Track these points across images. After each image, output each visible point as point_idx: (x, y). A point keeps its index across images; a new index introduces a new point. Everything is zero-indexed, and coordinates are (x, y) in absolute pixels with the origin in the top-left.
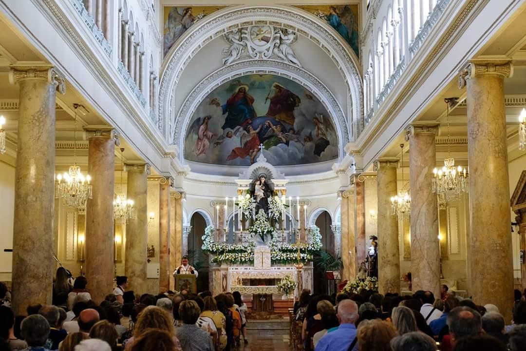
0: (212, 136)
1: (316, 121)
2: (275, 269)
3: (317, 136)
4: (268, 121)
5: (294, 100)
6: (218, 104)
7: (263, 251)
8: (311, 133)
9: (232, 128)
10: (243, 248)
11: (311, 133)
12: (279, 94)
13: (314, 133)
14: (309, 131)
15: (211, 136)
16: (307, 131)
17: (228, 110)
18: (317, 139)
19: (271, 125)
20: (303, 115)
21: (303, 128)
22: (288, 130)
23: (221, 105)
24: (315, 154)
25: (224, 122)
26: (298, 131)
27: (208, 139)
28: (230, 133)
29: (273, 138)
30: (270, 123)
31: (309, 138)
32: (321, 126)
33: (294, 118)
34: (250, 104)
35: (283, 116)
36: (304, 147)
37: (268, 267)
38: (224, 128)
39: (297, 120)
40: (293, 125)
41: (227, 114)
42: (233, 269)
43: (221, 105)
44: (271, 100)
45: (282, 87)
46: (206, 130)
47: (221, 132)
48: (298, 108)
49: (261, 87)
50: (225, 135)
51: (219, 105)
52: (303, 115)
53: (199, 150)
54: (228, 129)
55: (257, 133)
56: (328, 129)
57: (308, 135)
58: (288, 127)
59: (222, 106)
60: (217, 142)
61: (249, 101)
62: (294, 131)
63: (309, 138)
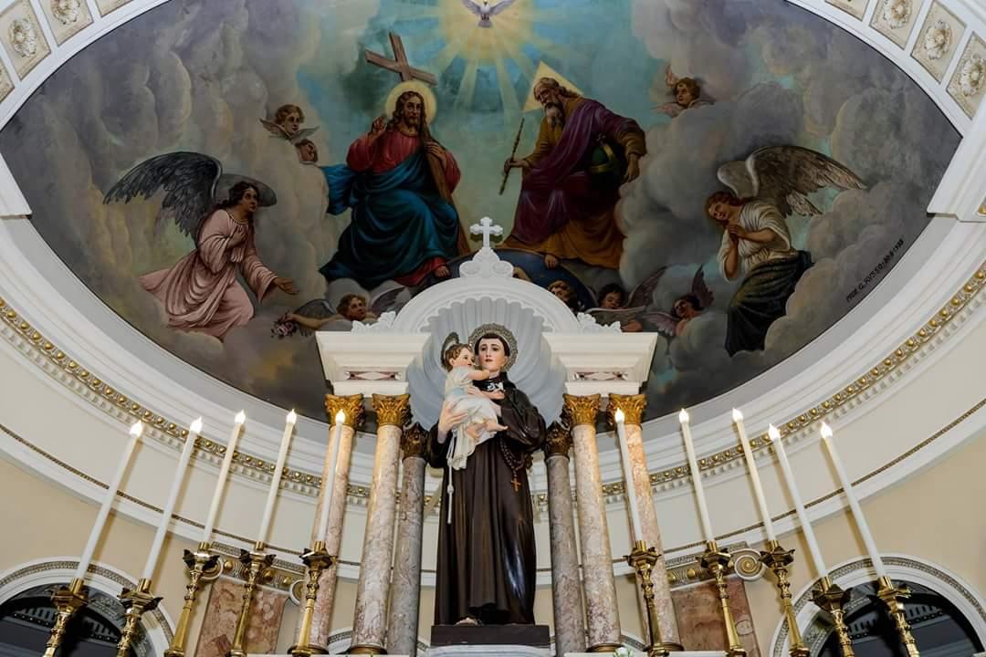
0: (272, 285)
1: (724, 207)
5: (619, 150)
6: (308, 152)
8: (700, 274)
9: (369, 285)
11: (700, 274)
12: (558, 135)
13: (716, 266)
14: (692, 270)
15: (265, 285)
16: (680, 275)
17: (353, 200)
18: (733, 284)
22: (595, 298)
23: (322, 161)
24: (732, 349)
25: (333, 249)
26: (642, 288)
27: (253, 290)
28: (355, 301)
31: (697, 298)
33: (619, 237)
34: (443, 190)
35: (574, 240)
36: (674, 343)
38: (330, 272)
39: (631, 244)
40: (616, 270)
41: (345, 218)
43: (322, 161)
44: (525, 170)
45: (570, 87)
46: (246, 242)
47: (315, 286)
48: (637, 182)
49: (486, 102)
50: (334, 305)
51: (315, 159)
53: (190, 310)
54: (349, 286)
56: (791, 199)
57: (686, 288)
58: (593, 281)
59: (325, 170)
60: (294, 321)
61: (438, 175)
62: (623, 294)
63: (697, 298)
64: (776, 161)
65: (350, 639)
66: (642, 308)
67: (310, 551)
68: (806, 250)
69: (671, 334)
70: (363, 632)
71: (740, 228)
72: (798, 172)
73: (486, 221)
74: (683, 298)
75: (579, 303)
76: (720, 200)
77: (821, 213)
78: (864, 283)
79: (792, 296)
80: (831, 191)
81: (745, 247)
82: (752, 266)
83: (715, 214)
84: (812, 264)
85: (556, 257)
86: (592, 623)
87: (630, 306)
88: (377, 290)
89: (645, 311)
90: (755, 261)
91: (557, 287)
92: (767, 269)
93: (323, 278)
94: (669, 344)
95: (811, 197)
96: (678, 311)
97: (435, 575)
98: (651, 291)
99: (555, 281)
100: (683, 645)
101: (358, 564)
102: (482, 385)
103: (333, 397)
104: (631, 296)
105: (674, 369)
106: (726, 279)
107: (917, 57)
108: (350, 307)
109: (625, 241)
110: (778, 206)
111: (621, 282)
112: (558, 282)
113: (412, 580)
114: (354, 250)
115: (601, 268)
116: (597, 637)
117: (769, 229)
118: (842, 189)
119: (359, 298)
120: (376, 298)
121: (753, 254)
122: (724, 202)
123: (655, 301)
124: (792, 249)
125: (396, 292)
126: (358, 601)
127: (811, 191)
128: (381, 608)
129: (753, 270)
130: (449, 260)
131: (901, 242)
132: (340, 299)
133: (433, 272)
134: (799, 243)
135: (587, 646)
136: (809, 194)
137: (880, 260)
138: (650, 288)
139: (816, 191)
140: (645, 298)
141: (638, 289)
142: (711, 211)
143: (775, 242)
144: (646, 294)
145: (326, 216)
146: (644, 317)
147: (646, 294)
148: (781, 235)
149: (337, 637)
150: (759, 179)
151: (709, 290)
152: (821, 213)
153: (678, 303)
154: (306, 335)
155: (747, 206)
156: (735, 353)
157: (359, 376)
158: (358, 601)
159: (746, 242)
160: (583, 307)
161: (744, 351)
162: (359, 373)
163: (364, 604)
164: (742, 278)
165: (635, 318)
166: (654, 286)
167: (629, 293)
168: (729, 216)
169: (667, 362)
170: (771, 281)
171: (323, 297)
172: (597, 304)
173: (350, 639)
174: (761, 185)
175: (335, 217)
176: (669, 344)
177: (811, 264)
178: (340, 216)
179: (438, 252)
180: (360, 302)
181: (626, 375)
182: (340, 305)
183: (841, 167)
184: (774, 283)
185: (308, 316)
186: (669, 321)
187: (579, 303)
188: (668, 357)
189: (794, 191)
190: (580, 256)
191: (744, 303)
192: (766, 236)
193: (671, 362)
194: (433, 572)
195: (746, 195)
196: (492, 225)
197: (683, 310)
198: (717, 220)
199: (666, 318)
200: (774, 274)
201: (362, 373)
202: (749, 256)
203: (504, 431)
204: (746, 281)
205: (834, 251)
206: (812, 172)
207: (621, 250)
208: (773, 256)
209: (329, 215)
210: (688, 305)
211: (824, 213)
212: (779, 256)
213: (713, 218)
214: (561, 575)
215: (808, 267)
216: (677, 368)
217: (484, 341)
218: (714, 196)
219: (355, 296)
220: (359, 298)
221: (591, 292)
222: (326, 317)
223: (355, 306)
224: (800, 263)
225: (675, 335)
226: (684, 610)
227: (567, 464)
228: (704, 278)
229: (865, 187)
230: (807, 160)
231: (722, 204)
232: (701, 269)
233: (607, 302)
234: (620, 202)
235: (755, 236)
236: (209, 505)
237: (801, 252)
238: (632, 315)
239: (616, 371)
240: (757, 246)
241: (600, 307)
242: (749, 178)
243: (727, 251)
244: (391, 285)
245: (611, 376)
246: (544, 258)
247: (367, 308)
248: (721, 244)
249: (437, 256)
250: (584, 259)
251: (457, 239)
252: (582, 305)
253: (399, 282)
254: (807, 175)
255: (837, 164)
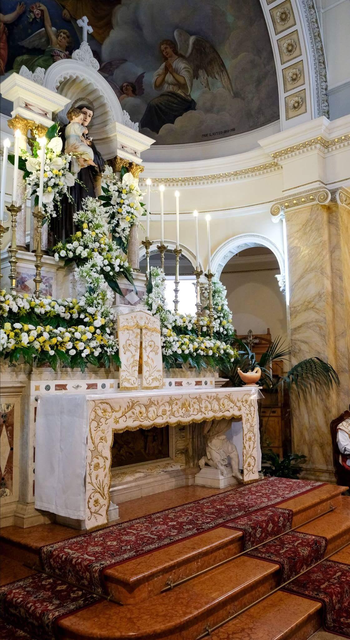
1: (169, 50)
2: (48, 388)
3: (159, 86)
4: (43, 7)
7: (142, 324)
8: (142, 76)
10: (60, 310)
11: (142, 76)
14: (140, 71)
19: (48, 22)
20: (137, 26)
21: (125, 60)
29: (44, 58)
30: (47, 15)
32: (180, 65)
37: (155, 379)
42: (48, 388)
52: (137, 26)
55: (6, 24)
56: (201, 72)
57: (133, 79)
64: (204, 49)
68: (195, 101)
71: (172, 66)
72: (210, 63)
74: (129, 83)
76: (169, 45)
77: (210, 90)
78: (212, 134)
79: (180, 117)
80: (219, 84)
81: (169, 78)
82: (169, 90)
83: (163, 51)
84: (195, 110)
85: (70, 14)
90: (171, 88)
92: (175, 96)
95: (210, 79)
96: (124, 88)
106: (154, 89)
107: (284, 72)
109: (112, 31)
110: (193, 71)
112: (66, 31)
117: (184, 77)
118: (224, 87)
121: (172, 84)
122: (171, 48)
124: (189, 95)
127: (211, 76)
129: (169, 92)
131: (234, 130)
134: (195, 95)
136: (210, 77)
137: (223, 130)
138: (115, 67)
139: (213, 78)
140: (110, 70)
141: (108, 63)
142: (163, 47)
143: (183, 86)
144: (111, 69)
147: (111, 69)
148: (188, 85)
150: (192, 51)
151: (143, 87)
152: (210, 90)
153: (125, 84)
155: (181, 58)
156: (143, 127)
159: (171, 76)
161: (148, 129)
164: (162, 92)
166: (117, 67)
168: (170, 57)
170: (174, 103)
174: (191, 54)
177: (194, 109)
183: (229, 77)
184: (175, 105)
189: (204, 70)
191: (157, 105)
192: (181, 80)
195: (183, 54)
197: (127, 89)
198: (163, 54)
200: (176, 101)
202: (169, 84)
204: (162, 95)
205: (209, 110)
206: (216, 68)
207: (108, 34)
208: (179, 92)
210: (130, 88)
211: (212, 91)
212: (183, 95)
213: (162, 52)
215: (192, 109)
218: (168, 40)
224: (190, 105)
228: (144, 79)
229: (233, 95)
230: (217, 61)
231: (169, 48)
232: (144, 73)
234: (119, 6)
235: (178, 77)
236: (177, 237)
237: (193, 100)
240: (176, 82)
242: (188, 45)
243: (160, 73)
248: (158, 68)
254: (213, 68)
255: (228, 75)
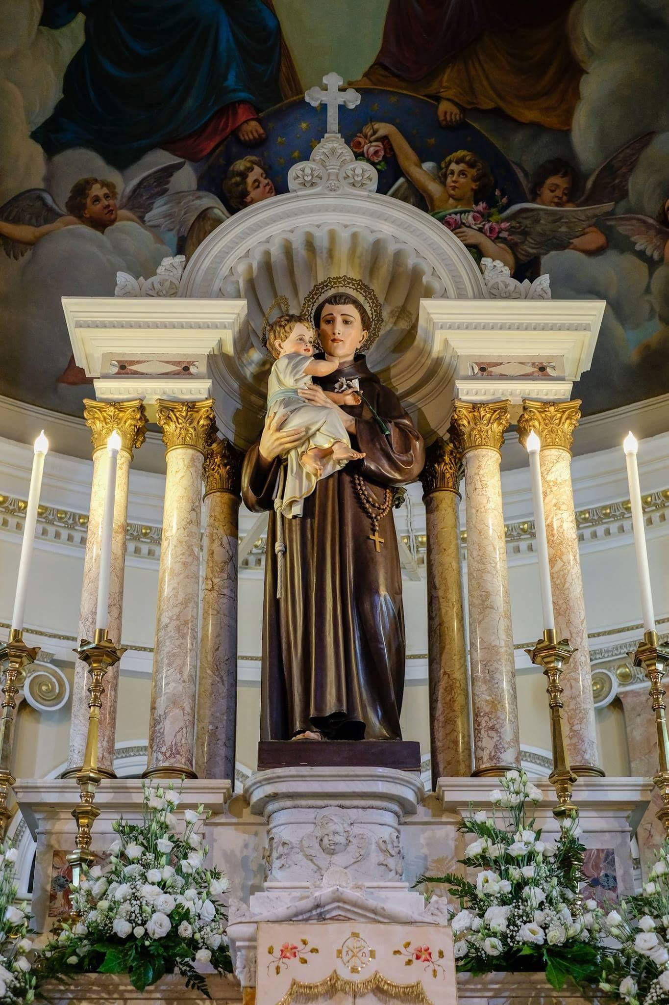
26: (609, 170)
28: (97, 190)
40: (565, 134)
50: (59, 200)
65: (146, 758)
66: (608, 206)
67: (89, 643)
69: (656, 256)
70: (163, 749)
73: (333, 80)
75: (497, 193)
86: (480, 740)
87: (586, 203)
88: (133, 168)
89: (612, 213)
91: (458, 162)
93: (38, 150)
94: (651, 275)
97: (239, 654)
98: (625, 177)
99: (456, 151)
100: (606, 773)
101: (151, 650)
102: (326, 383)
103: (94, 403)
104: (589, 184)
105: (656, 321)
108: (89, 201)
111: (573, 155)
112: (460, 153)
113: (225, 678)
114: (92, 94)
115: (537, 128)
116: (486, 757)
119: (104, 184)
120: (135, 181)
123: (630, 193)
125: (169, 171)
126: (153, 708)
128: (187, 718)
130: (262, 111)
132: (70, 187)
133: (235, 133)
135: (474, 768)
145: (39, 32)
146: (610, 223)
149: (127, 752)
154: (16, 258)
157: (134, 368)
158: (153, 708)
160: (505, 200)
162: (133, 363)
163: (162, 713)
165: (594, 225)
166: (632, 166)
167: (586, 177)
169: (647, 308)
171: (42, 185)
172: (529, 197)
173: (146, 758)
175: (56, 33)
176: (651, 275)
178: (65, 30)
179: (244, 95)
180: (105, 190)
181: (554, 368)
182: (71, 198)
185: (17, 220)
186: (652, 233)
187: (497, 193)
188: (647, 297)
190: (501, 104)
193: (652, 310)
194: (243, 658)
196: (342, 108)
199: (649, 226)
201: (138, 362)
203: (361, 461)
207: (577, 95)
209: (43, 28)
214: (442, 671)
216: (661, 318)
217: (328, 309)
219: (96, 181)
220: (104, 184)
221: (521, 175)
222: (46, 222)
223: (97, 199)
225: (662, 260)
226: (638, 720)
227: (457, 505)
233: (546, 194)
238: (588, 218)
239: (537, 361)
241: (533, 201)
244: (160, 159)
245: (529, 370)
246: (437, 107)
247: (118, 203)
249: (242, 102)
250: (509, 110)
251: (279, 69)
252: (503, 196)
253: (174, 152)
